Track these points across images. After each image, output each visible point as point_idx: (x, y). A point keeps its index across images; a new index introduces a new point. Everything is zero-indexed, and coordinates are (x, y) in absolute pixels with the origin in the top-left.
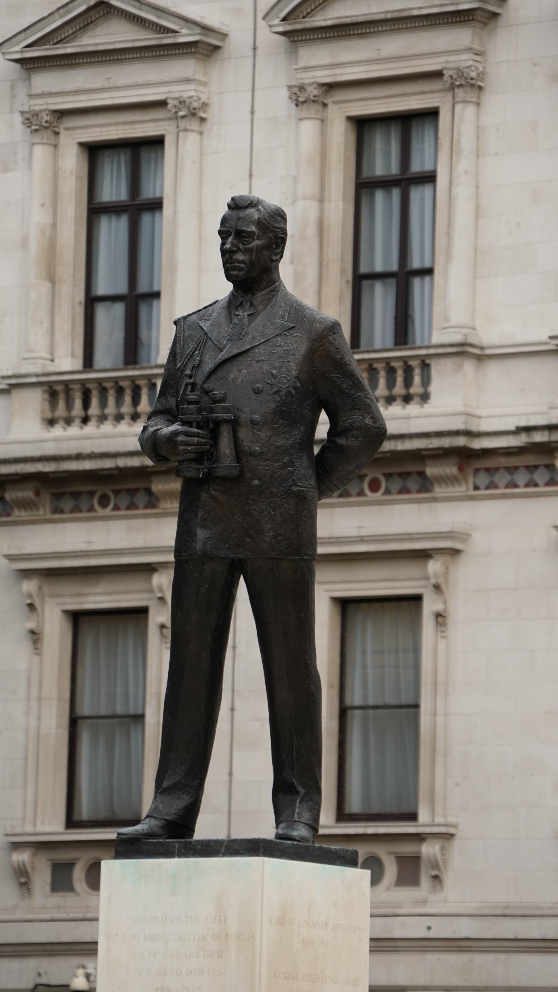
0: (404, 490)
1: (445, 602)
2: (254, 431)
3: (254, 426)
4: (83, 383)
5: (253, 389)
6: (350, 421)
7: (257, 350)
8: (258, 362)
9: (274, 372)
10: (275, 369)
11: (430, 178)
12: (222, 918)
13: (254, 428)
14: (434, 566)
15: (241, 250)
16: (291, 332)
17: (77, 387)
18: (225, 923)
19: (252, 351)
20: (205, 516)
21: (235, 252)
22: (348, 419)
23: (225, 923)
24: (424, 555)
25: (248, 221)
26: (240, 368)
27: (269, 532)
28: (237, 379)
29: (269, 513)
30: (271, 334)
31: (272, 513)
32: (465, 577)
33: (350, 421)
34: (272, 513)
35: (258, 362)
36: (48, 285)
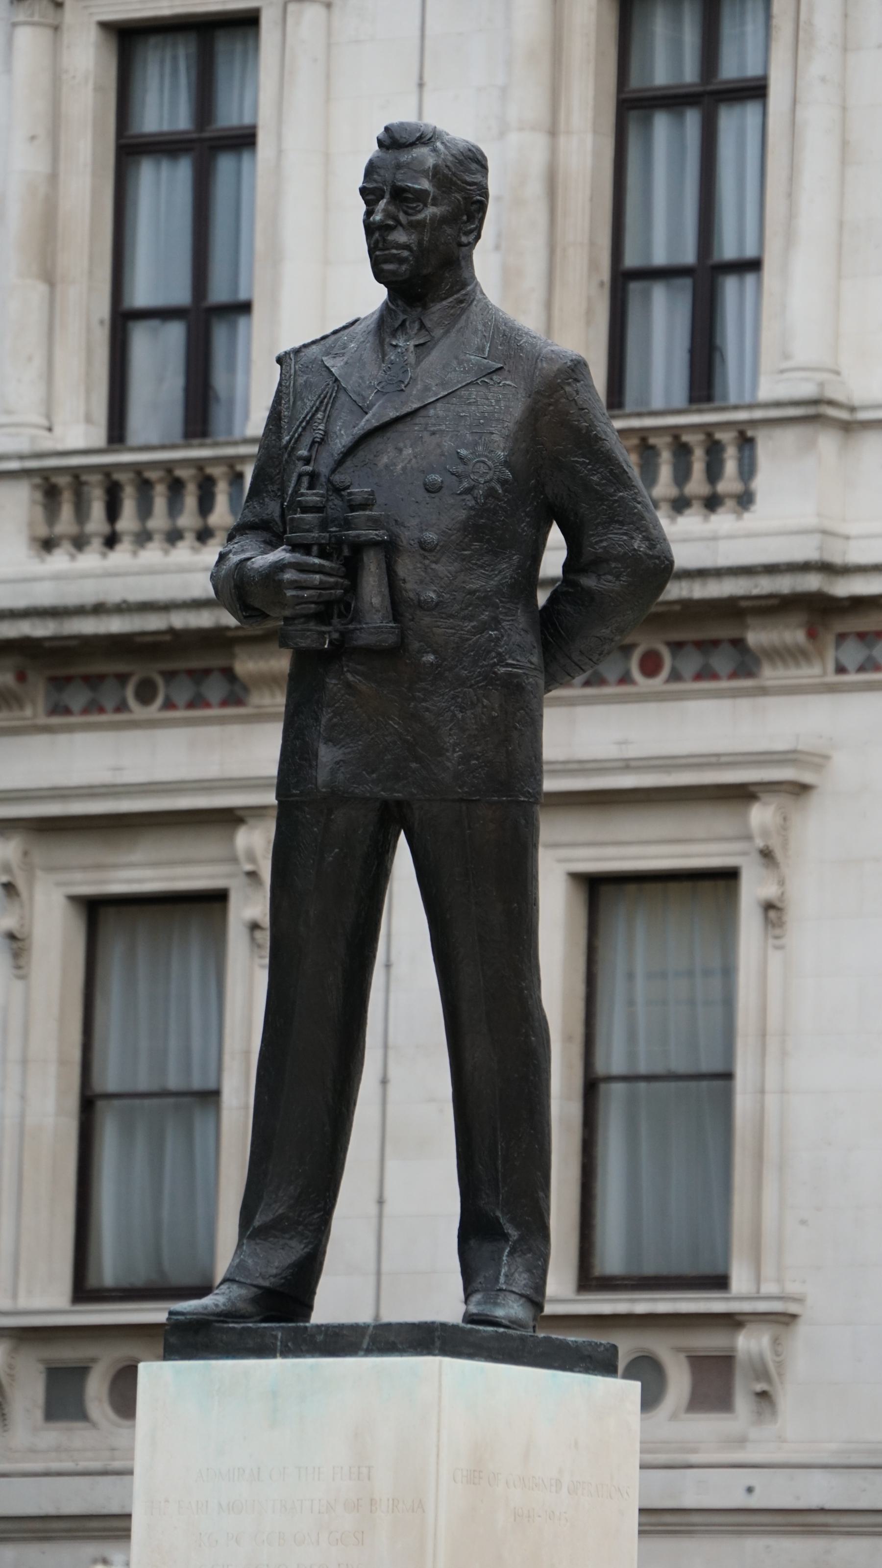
0: (705, 674)
1: (782, 883)
2: (427, 562)
3: (426, 554)
4: (106, 471)
5: (425, 484)
6: (605, 544)
7: (432, 412)
8: (433, 433)
9: (463, 452)
10: (466, 446)
11: (755, 91)
12: (364, 1470)
13: (425, 557)
14: (761, 815)
15: (401, 225)
16: (495, 377)
17: (95, 478)
18: (369, 1479)
19: (423, 413)
20: (335, 720)
21: (390, 229)
22: (601, 541)
23: (369, 1479)
24: (742, 794)
25: (415, 171)
26: (401, 445)
27: (454, 751)
28: (395, 465)
29: (454, 715)
30: (458, 382)
31: (460, 716)
32: (818, 837)
33: (605, 544)
34: (460, 716)
35: (433, 433)
36: (42, 288)
